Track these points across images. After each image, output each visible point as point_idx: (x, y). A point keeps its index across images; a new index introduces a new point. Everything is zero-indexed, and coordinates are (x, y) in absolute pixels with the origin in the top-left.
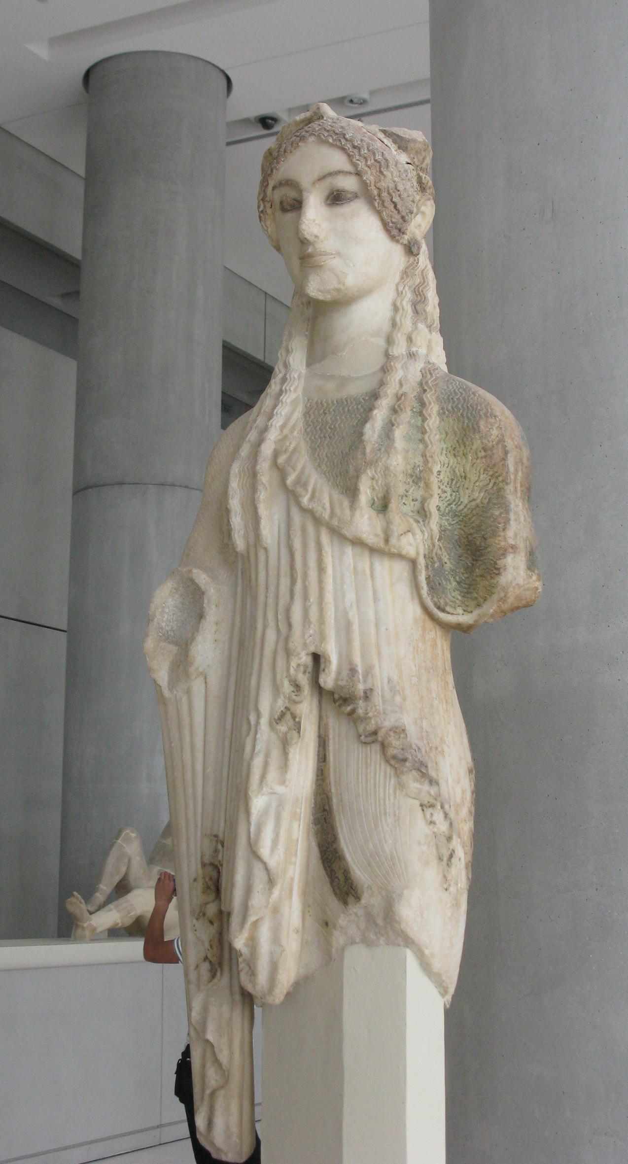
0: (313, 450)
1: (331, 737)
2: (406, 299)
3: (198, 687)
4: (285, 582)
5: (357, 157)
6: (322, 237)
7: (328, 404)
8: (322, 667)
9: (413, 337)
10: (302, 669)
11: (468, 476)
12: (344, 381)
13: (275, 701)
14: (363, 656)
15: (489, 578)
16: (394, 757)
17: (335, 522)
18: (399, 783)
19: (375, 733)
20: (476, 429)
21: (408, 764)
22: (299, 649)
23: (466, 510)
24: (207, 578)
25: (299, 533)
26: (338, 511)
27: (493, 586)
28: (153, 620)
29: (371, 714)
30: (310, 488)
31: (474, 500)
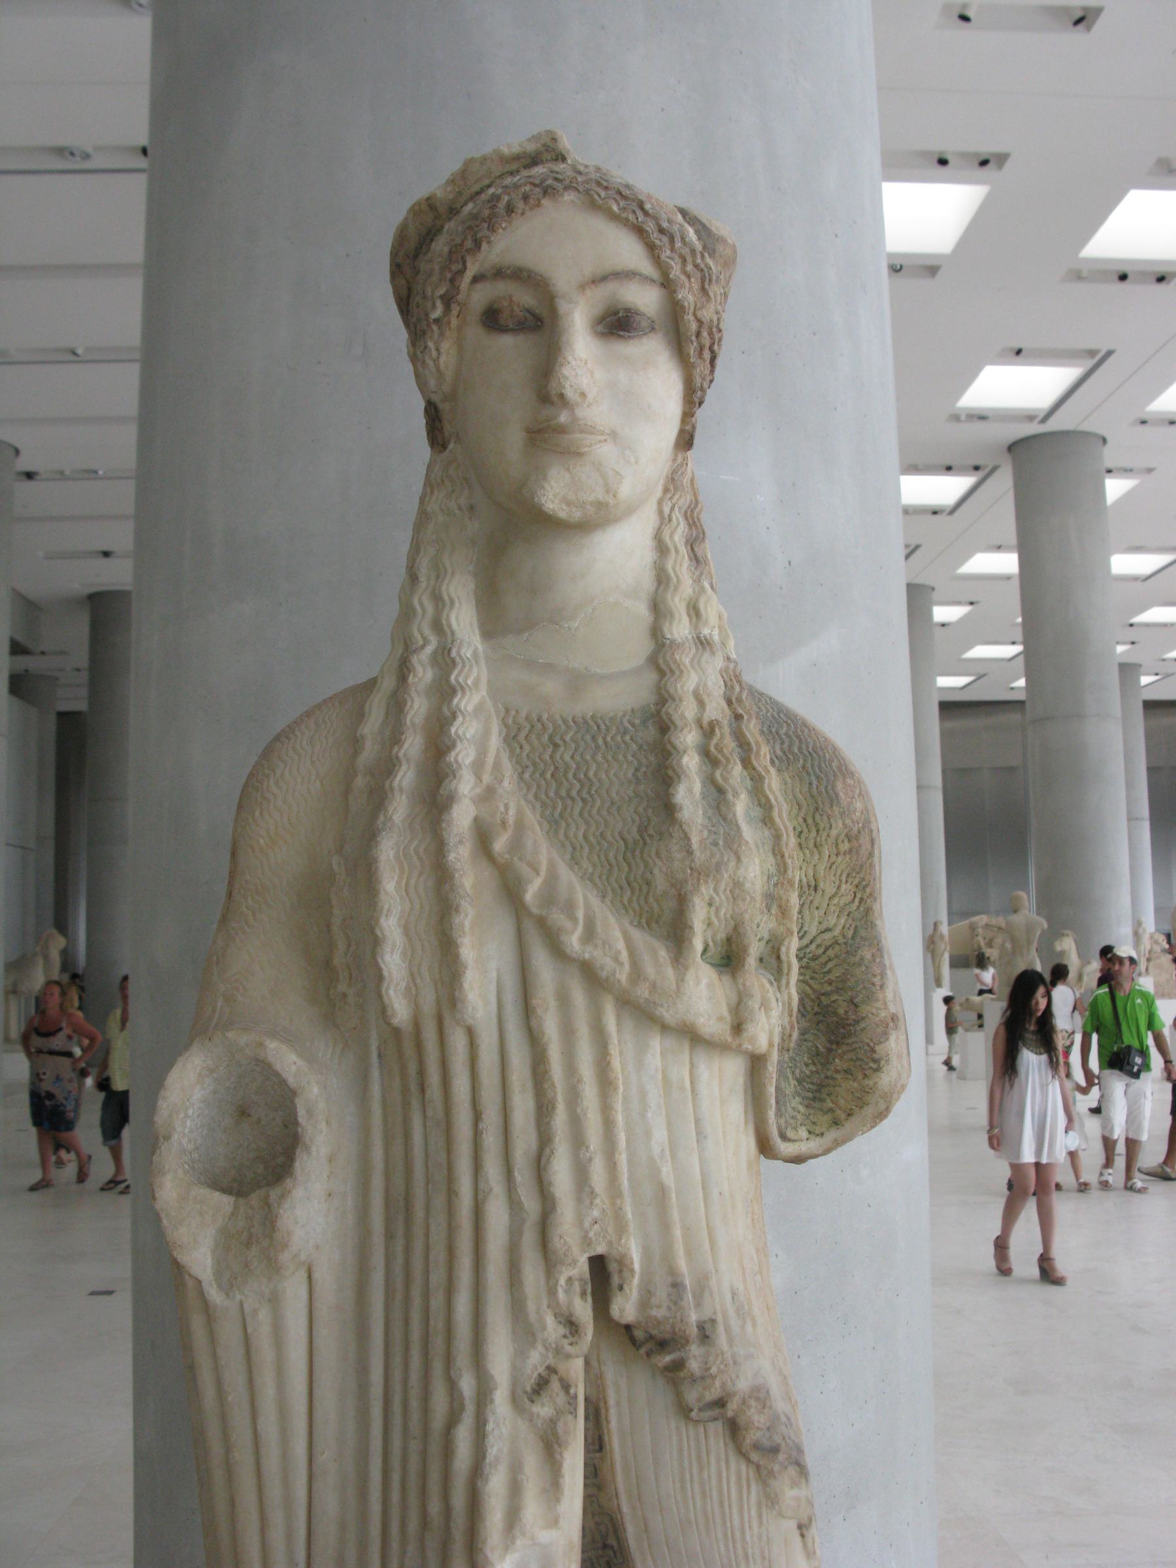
0: (553, 824)
1: (611, 1402)
2: (679, 532)
3: (294, 1290)
4: (523, 1106)
5: (668, 253)
6: (590, 397)
7: (556, 726)
8: (615, 1280)
9: (701, 606)
10: (577, 1287)
11: (821, 884)
12: (578, 682)
13: (520, 1354)
14: (689, 1253)
15: (860, 1077)
16: (756, 1446)
17: (642, 992)
18: (767, 1496)
19: (720, 1403)
20: (833, 799)
21: (781, 1457)
22: (575, 1250)
23: (813, 946)
24: (300, 1062)
25: (552, 1004)
26: (650, 970)
27: (866, 1091)
28: (167, 1138)
29: (714, 1370)
30: (580, 914)
31: (828, 930)
